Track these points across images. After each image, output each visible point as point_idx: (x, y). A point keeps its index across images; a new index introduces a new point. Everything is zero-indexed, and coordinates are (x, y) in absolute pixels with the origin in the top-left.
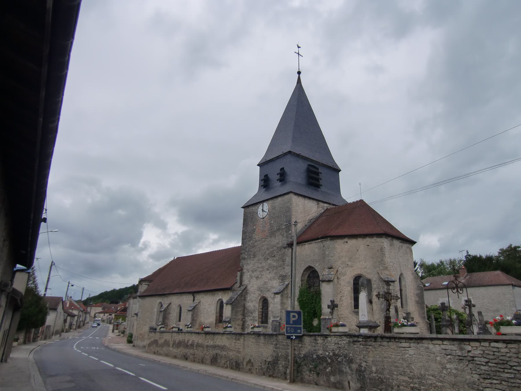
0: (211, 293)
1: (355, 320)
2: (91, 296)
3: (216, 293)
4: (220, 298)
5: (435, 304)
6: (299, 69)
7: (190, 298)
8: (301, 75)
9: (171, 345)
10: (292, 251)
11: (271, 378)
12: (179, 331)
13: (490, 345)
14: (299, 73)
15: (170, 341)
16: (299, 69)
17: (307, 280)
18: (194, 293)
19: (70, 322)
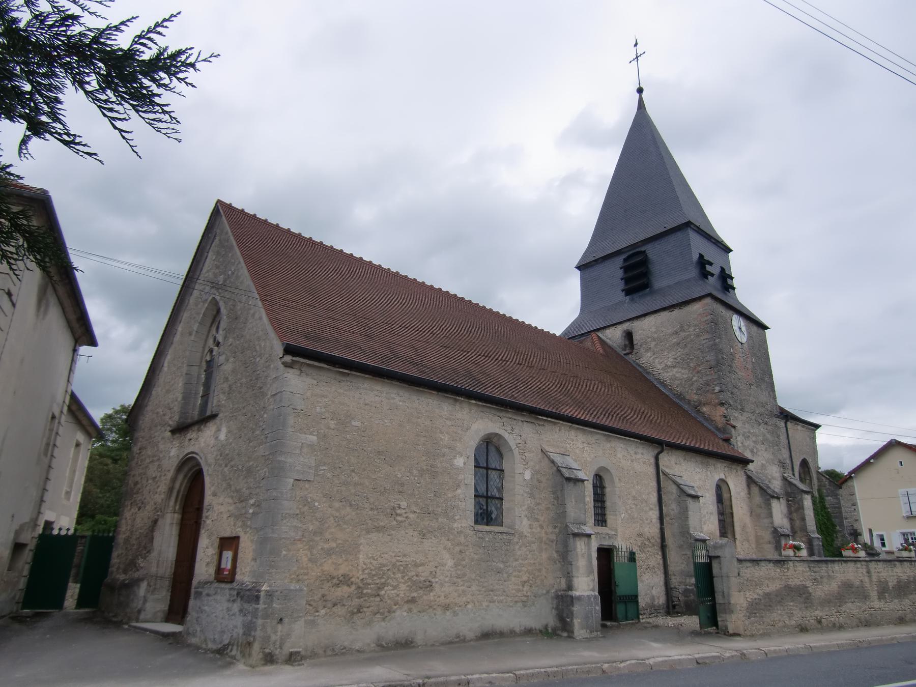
0: (699, 458)
1: (676, 524)
2: (78, 274)
3: (712, 461)
4: (722, 476)
5: (606, 483)
6: (639, 84)
7: (639, 456)
8: (644, 95)
9: (874, 594)
10: (92, 80)
11: (866, 628)
12: (905, 554)
13: (795, 554)
14: (640, 90)
15: (867, 585)
16: (639, 84)
17: (194, 289)
18: (661, 445)
19: (588, 640)
